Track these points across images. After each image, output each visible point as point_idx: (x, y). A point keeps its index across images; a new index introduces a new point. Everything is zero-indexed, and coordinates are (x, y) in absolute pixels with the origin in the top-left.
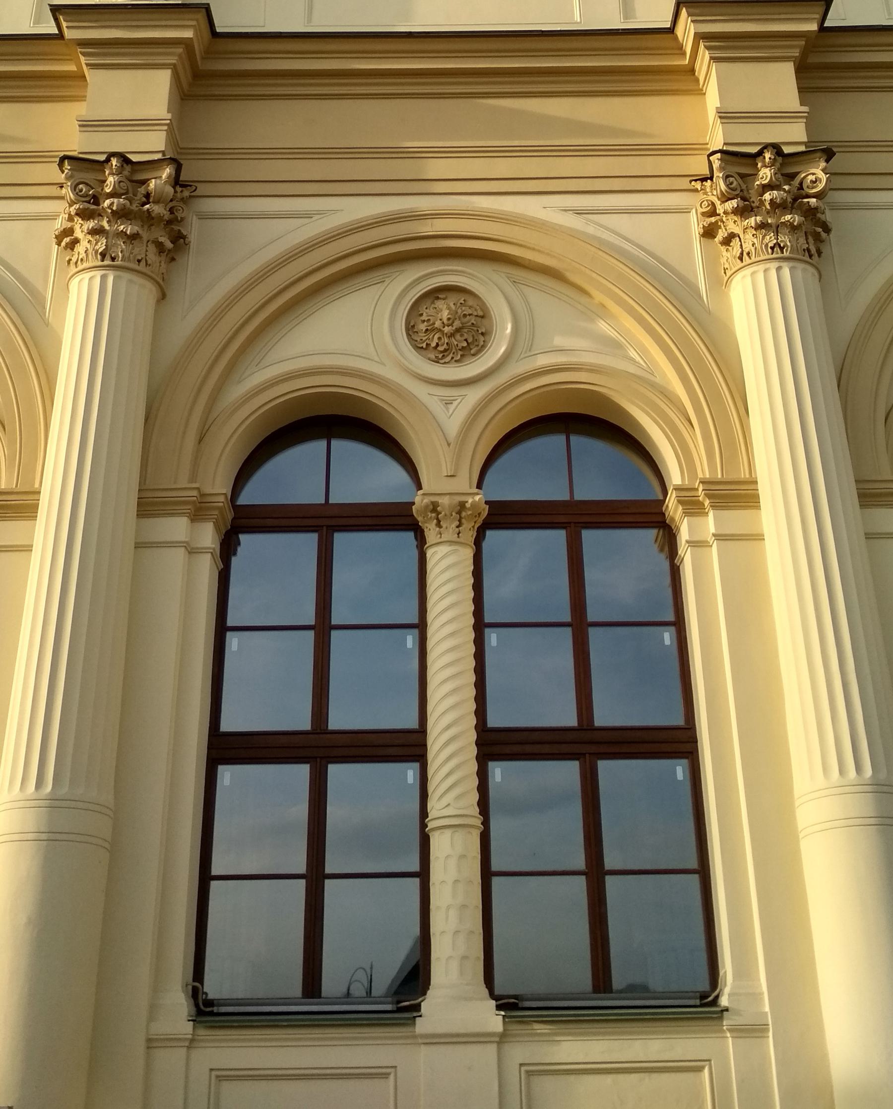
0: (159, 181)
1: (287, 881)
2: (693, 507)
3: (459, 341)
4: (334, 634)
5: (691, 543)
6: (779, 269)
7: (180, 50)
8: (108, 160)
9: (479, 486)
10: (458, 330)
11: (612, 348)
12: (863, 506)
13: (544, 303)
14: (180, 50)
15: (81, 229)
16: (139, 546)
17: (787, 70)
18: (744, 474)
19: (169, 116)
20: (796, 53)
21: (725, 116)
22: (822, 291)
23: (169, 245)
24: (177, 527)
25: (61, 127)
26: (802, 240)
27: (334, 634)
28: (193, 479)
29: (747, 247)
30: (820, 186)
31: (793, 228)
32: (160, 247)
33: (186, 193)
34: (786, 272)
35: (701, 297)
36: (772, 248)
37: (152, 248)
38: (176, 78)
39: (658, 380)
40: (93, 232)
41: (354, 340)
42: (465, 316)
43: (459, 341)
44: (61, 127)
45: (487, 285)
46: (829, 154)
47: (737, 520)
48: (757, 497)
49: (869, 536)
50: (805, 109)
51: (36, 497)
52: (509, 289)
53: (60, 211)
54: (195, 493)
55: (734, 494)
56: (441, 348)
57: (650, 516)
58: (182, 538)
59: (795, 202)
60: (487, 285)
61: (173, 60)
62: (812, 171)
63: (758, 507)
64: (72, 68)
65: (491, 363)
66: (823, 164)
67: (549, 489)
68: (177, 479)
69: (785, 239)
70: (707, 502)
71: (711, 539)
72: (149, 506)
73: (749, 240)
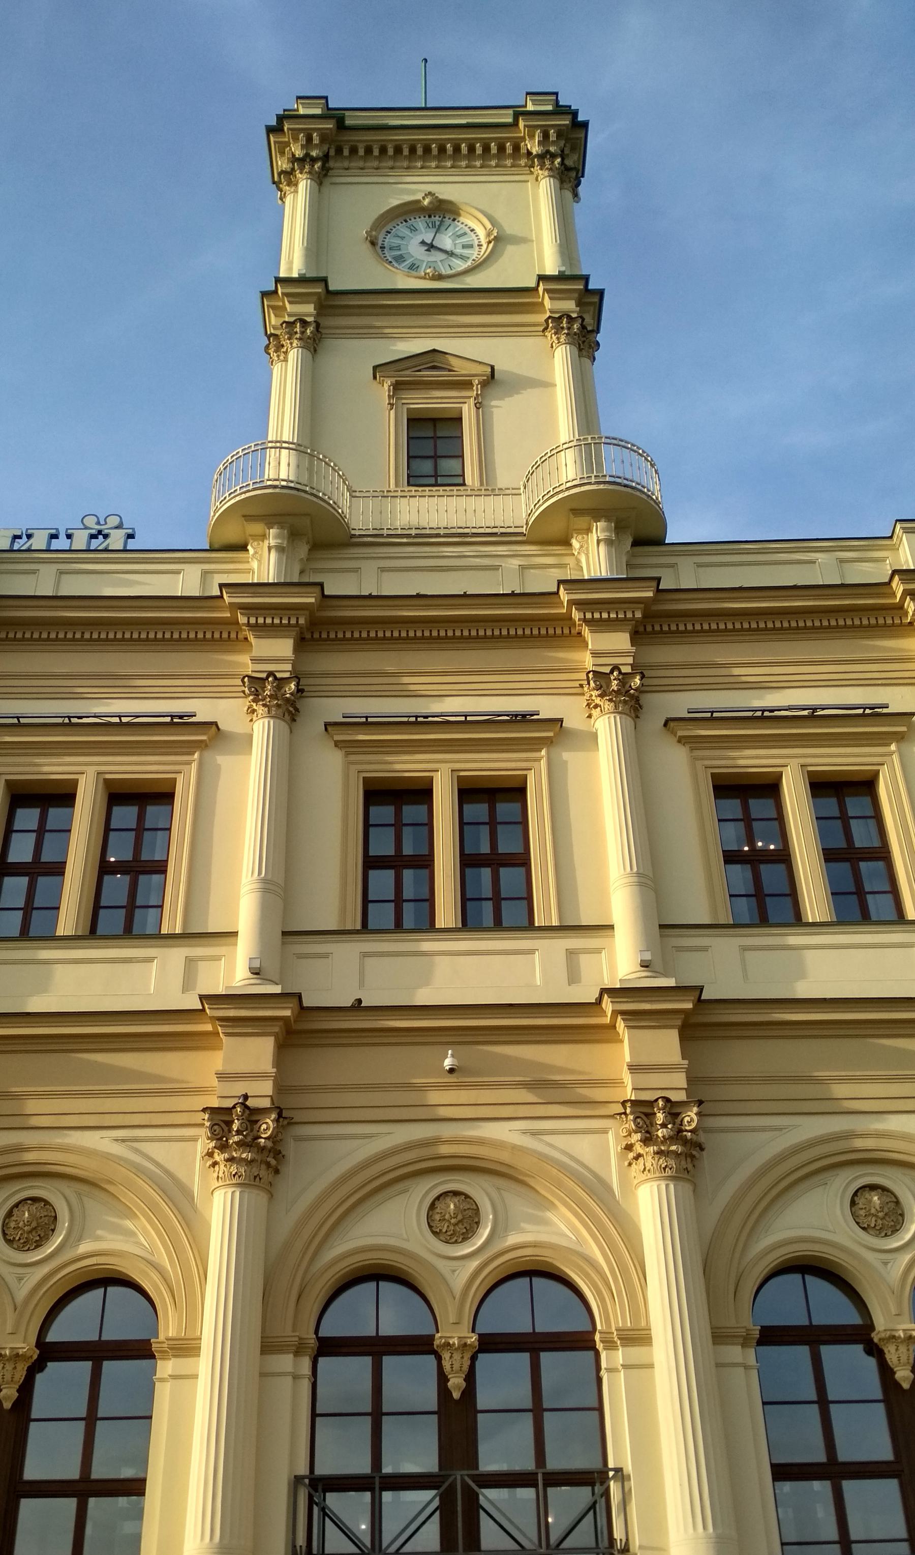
0: (268, 1125)
1: (384, 362)
2: (610, 1345)
3: (461, 1229)
4: (385, 1418)
5: (608, 1370)
6: (615, 717)
7: (281, 1023)
8: (267, 678)
9: (473, 1331)
10: (460, 1221)
11: (558, 1229)
12: (714, 1344)
13: (516, 1203)
14: (281, 1023)
15: (219, 1157)
16: (263, 1375)
17: (672, 1037)
18: (643, 1324)
19: (275, 1070)
20: (679, 1023)
21: (633, 1068)
22: (636, 738)
23: (273, 1162)
24: (286, 1362)
25: (244, 663)
26: (683, 1162)
27: (385, 1418)
28: (294, 1331)
29: (648, 1166)
30: (694, 1125)
31: (677, 1154)
32: (268, 1165)
33: (286, 1122)
34: (672, 1186)
35: (614, 1193)
36: (664, 1169)
37: (263, 1166)
38: (276, 1041)
39: (587, 1252)
40: (227, 1160)
41: (396, 1226)
42: (465, 1210)
43: (461, 1229)
44: (244, 663)
45: (477, 1188)
46: (700, 1103)
47: (636, 1353)
48: (651, 1338)
49: (718, 1365)
50: (686, 1062)
51: (198, 1342)
52: (494, 1194)
53: (204, 1143)
54: (297, 1339)
55: (637, 1337)
56: (449, 1233)
57: (581, 1342)
58: (290, 1369)
59: (678, 1135)
60: (477, 1188)
61: (276, 1029)
62: (689, 1113)
63: (651, 1345)
64: (281, 304)
65: (480, 1242)
66: (695, 1109)
67: (517, 1322)
68: (285, 1330)
69: (672, 1163)
70: (616, 1339)
71: (620, 1368)
72: (268, 1347)
73: (649, 1161)
